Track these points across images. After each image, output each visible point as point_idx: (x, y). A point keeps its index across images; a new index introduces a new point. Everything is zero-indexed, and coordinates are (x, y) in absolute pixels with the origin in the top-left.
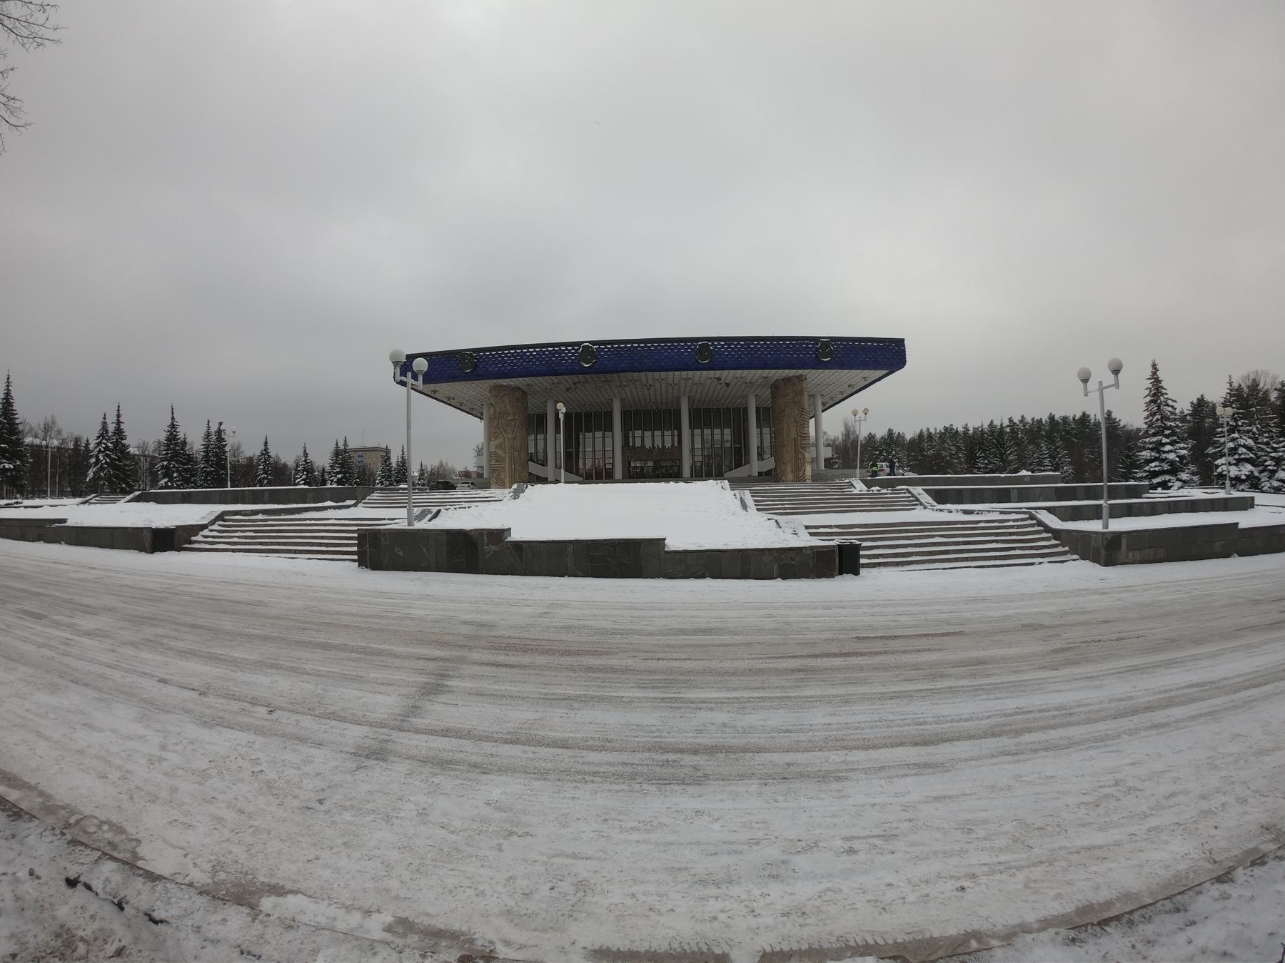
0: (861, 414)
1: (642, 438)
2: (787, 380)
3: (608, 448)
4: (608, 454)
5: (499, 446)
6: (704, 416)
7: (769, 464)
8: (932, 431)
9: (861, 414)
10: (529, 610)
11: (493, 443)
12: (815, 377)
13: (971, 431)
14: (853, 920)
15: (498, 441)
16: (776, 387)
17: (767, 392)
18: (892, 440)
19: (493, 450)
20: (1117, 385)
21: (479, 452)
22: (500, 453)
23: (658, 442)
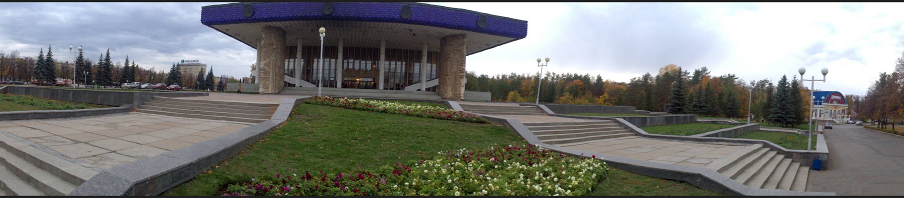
0: (543, 62)
1: (354, 63)
2: (453, 36)
3: (333, 68)
4: (333, 72)
5: (267, 65)
6: (393, 54)
7: (435, 82)
8: (216, 74)
9: (543, 62)
10: (85, 164)
11: (262, 63)
12: (471, 36)
13: (550, 79)
14: (660, 195)
15: (267, 61)
16: (444, 40)
17: (437, 44)
18: (483, 79)
19: (262, 66)
20: (824, 81)
21: (254, 68)
22: (267, 68)
23: (357, 67)
